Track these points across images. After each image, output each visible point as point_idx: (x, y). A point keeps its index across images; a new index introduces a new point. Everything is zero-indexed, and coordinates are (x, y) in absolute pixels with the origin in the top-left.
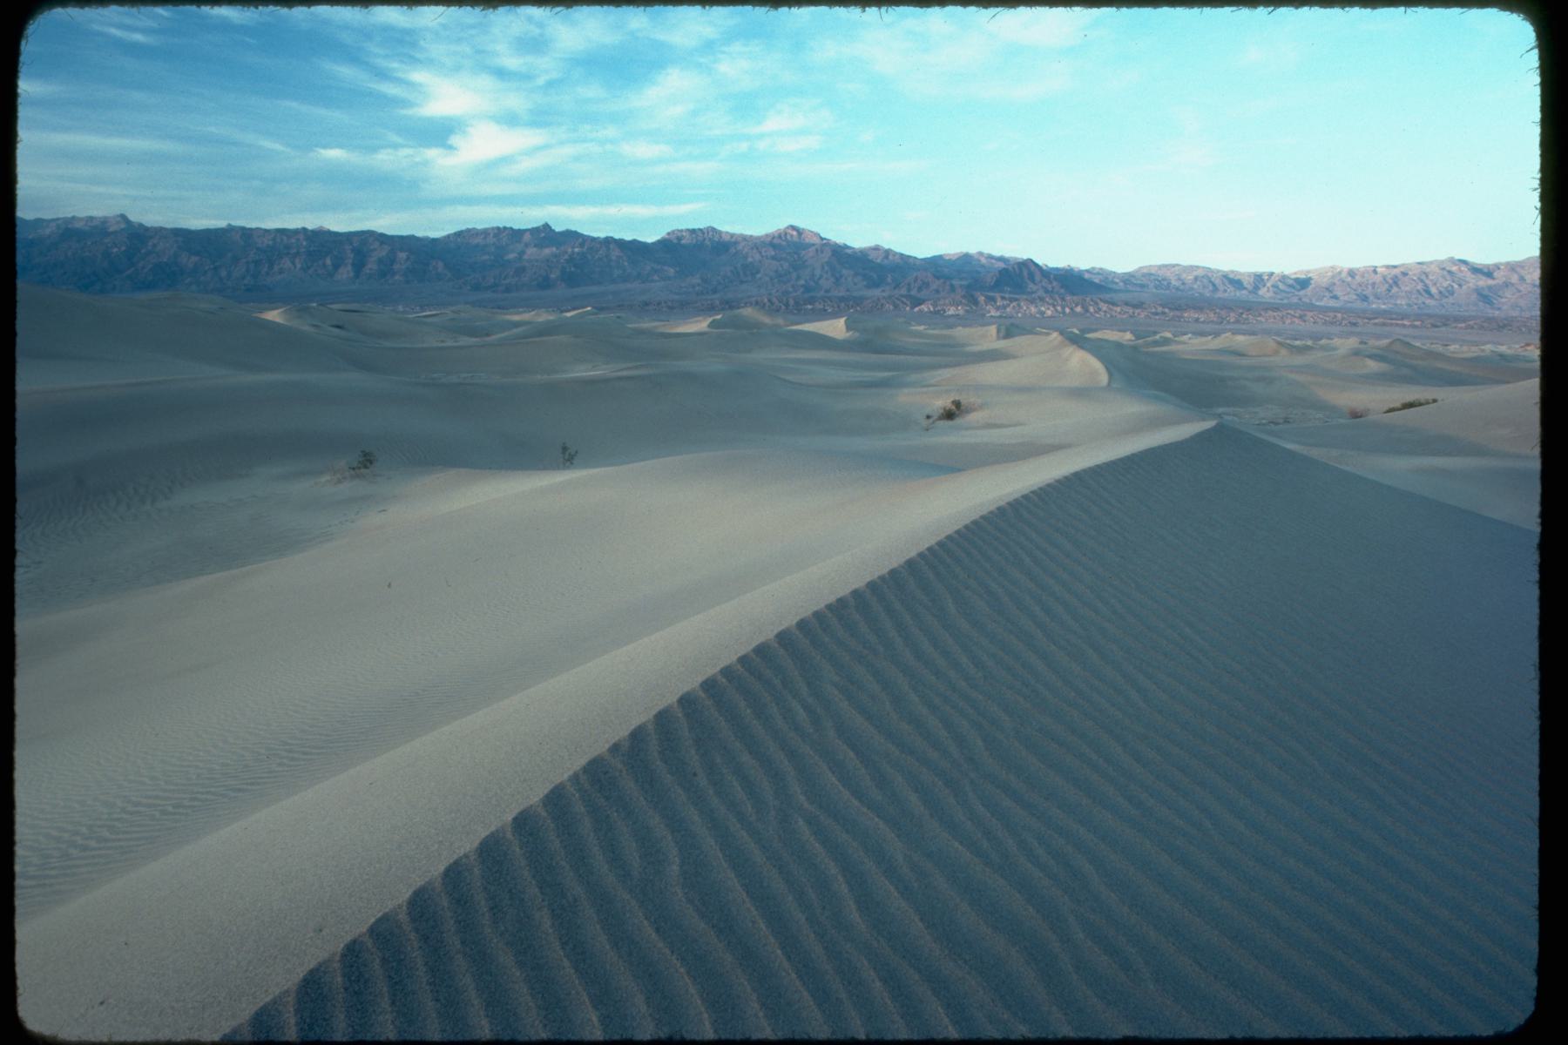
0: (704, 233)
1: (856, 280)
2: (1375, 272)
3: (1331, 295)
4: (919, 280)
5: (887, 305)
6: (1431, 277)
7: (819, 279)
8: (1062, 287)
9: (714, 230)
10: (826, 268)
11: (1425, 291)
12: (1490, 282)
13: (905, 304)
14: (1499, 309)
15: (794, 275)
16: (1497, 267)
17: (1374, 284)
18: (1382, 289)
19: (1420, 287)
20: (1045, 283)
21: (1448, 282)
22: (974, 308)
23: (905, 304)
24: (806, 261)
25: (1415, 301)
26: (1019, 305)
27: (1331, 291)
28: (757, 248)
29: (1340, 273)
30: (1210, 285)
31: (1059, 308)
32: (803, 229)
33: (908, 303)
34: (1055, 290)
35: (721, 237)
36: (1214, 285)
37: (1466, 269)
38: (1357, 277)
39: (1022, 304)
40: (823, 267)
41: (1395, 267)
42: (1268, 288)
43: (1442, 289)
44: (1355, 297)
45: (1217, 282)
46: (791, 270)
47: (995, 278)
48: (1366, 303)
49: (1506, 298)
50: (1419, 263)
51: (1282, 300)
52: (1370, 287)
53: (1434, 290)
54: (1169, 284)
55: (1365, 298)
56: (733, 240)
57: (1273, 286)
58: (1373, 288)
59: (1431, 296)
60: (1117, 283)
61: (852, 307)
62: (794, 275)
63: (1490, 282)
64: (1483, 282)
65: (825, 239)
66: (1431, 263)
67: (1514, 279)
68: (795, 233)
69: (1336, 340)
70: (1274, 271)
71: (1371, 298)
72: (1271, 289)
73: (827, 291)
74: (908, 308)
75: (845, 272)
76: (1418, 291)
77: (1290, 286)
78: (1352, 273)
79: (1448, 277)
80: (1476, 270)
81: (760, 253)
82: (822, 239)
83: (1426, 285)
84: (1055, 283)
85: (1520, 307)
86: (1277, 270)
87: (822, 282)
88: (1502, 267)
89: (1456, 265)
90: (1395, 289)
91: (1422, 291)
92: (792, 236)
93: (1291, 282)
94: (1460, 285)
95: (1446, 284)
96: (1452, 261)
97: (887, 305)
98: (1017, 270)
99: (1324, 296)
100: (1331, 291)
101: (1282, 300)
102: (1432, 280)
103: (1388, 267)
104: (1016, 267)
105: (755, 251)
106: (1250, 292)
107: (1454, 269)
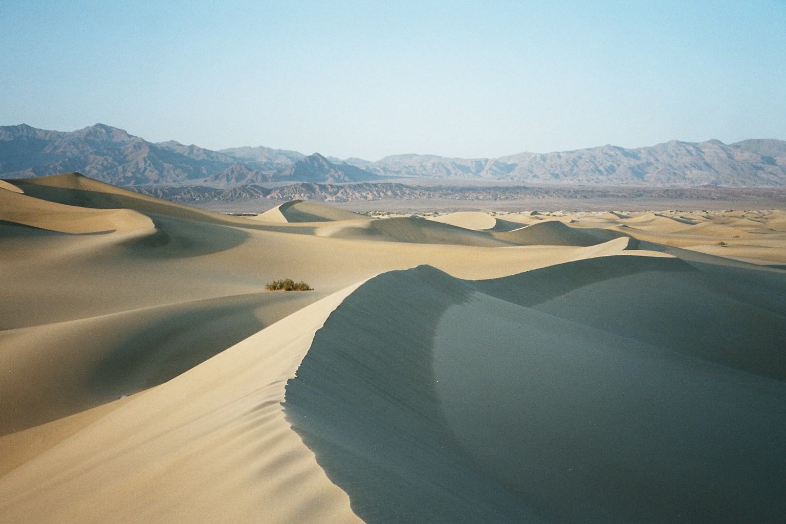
0: (18, 131)
1: (177, 172)
2: (559, 157)
3: (533, 174)
4: (235, 172)
5: (244, 194)
6: (598, 160)
7: (144, 172)
8: (712, 211)
9: (28, 127)
10: (149, 162)
11: (596, 169)
12: (638, 162)
13: (258, 193)
14: (648, 181)
15: (120, 169)
16: (639, 150)
17: (561, 166)
18: (567, 169)
19: (592, 167)
20: (333, 171)
21: (610, 163)
22: (313, 194)
23: (258, 193)
24: (127, 156)
25: (592, 177)
26: (345, 191)
27: (532, 172)
28: (74, 144)
29: (535, 158)
30: (445, 170)
31: (375, 193)
32: (111, 127)
33: (260, 192)
34: (342, 178)
35: (35, 134)
36: (447, 170)
37: (620, 153)
38: (548, 161)
39: (348, 190)
40: (146, 162)
41: (571, 152)
42: (487, 171)
43: (607, 168)
44: (549, 175)
45: (450, 167)
46: (116, 163)
47: (293, 169)
48: (558, 180)
49: (650, 173)
50: (588, 149)
51: (499, 179)
52: (558, 168)
53: (601, 168)
54: (415, 170)
55: (557, 176)
56: (48, 138)
57: (490, 169)
58: (561, 168)
59: (600, 172)
60: (378, 171)
61: (215, 196)
62: (120, 169)
63: (638, 162)
64: (634, 163)
65: (132, 136)
66: (596, 149)
67: (652, 160)
68: (103, 131)
69: (444, 215)
70: (488, 158)
71: (561, 175)
72: (489, 171)
73: (156, 182)
74: (261, 196)
75: (166, 165)
76: (591, 169)
77: (501, 169)
78: (543, 158)
79: (609, 159)
80: (627, 154)
81: (78, 148)
82: (130, 136)
83: (596, 166)
84: (340, 173)
85: (661, 180)
86: (490, 157)
87: (147, 173)
88: (642, 151)
89: (612, 150)
90: (576, 170)
91: (594, 169)
92: (101, 133)
93: (502, 166)
94: (619, 165)
95: (609, 164)
96: (609, 146)
97: (244, 194)
98: (308, 161)
99: (528, 176)
100: (532, 172)
101: (499, 179)
102: (599, 162)
103: (567, 152)
104: (308, 159)
105: (72, 146)
106: (474, 174)
107: (612, 153)
